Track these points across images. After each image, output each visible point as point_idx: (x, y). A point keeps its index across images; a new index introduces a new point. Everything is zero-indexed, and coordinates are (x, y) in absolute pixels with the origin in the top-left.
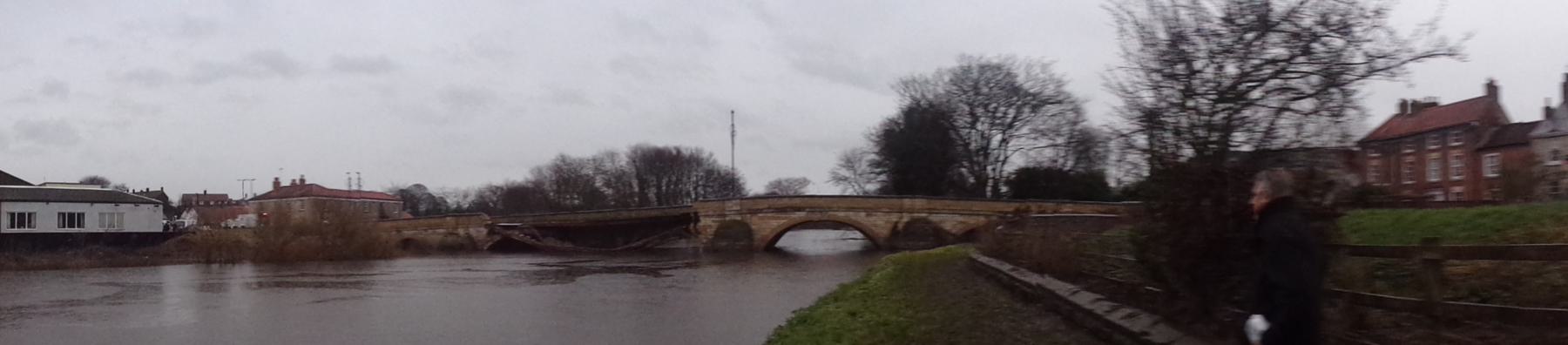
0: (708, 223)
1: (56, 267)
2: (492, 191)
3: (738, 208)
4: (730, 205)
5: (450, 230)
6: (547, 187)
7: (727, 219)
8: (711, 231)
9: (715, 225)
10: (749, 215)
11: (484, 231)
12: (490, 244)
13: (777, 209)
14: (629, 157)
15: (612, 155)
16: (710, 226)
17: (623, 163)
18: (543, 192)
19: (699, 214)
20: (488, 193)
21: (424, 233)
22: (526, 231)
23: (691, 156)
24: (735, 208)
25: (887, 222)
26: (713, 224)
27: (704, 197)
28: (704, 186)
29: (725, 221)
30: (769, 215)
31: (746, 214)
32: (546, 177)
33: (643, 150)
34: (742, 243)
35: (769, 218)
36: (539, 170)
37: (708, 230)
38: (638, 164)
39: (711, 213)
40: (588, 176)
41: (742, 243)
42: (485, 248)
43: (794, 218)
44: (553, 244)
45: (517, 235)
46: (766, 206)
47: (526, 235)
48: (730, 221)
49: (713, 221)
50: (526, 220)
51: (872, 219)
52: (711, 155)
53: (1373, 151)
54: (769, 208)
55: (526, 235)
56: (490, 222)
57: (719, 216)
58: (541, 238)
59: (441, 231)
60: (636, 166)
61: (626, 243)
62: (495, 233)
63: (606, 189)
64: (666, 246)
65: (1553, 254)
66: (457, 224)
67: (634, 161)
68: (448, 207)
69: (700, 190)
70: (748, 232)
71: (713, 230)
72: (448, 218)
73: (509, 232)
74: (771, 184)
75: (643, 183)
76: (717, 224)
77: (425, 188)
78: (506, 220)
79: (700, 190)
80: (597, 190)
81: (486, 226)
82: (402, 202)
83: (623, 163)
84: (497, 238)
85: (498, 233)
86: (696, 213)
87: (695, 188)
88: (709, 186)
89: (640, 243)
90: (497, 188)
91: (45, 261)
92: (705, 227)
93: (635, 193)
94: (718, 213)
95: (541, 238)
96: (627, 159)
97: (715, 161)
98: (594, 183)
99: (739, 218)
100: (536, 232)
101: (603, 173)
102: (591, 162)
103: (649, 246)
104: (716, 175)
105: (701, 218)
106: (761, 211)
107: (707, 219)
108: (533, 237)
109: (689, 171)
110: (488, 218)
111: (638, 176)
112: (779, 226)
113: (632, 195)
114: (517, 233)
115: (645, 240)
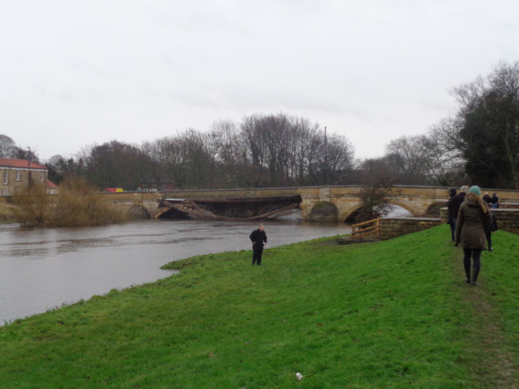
0: (308, 203)
3: (328, 193)
4: (323, 191)
5: (137, 203)
7: (321, 200)
8: (309, 209)
9: (313, 204)
10: (335, 198)
11: (157, 205)
12: (160, 214)
13: (352, 194)
15: (227, 127)
16: (309, 205)
19: (302, 197)
21: (113, 204)
24: (325, 193)
25: (424, 205)
29: (319, 202)
30: (349, 198)
31: (333, 197)
33: (257, 122)
34: (330, 217)
35: (349, 200)
37: (308, 208)
41: (330, 217)
42: (156, 217)
45: (181, 208)
46: (347, 192)
47: (188, 208)
49: (311, 202)
51: (412, 202)
54: (349, 194)
55: (188, 208)
57: (315, 198)
59: (128, 203)
61: (255, 214)
66: (142, 199)
70: (335, 210)
71: (311, 207)
73: (176, 206)
74: (393, 143)
75: (256, 153)
76: (313, 204)
77: (9, 140)
81: (158, 201)
82: (47, 171)
84: (165, 210)
85: (166, 206)
91: (237, 224)
92: (306, 206)
94: (314, 196)
96: (241, 130)
99: (328, 200)
100: (195, 205)
105: (304, 200)
106: (343, 195)
107: (307, 200)
111: (253, 147)
112: (355, 206)
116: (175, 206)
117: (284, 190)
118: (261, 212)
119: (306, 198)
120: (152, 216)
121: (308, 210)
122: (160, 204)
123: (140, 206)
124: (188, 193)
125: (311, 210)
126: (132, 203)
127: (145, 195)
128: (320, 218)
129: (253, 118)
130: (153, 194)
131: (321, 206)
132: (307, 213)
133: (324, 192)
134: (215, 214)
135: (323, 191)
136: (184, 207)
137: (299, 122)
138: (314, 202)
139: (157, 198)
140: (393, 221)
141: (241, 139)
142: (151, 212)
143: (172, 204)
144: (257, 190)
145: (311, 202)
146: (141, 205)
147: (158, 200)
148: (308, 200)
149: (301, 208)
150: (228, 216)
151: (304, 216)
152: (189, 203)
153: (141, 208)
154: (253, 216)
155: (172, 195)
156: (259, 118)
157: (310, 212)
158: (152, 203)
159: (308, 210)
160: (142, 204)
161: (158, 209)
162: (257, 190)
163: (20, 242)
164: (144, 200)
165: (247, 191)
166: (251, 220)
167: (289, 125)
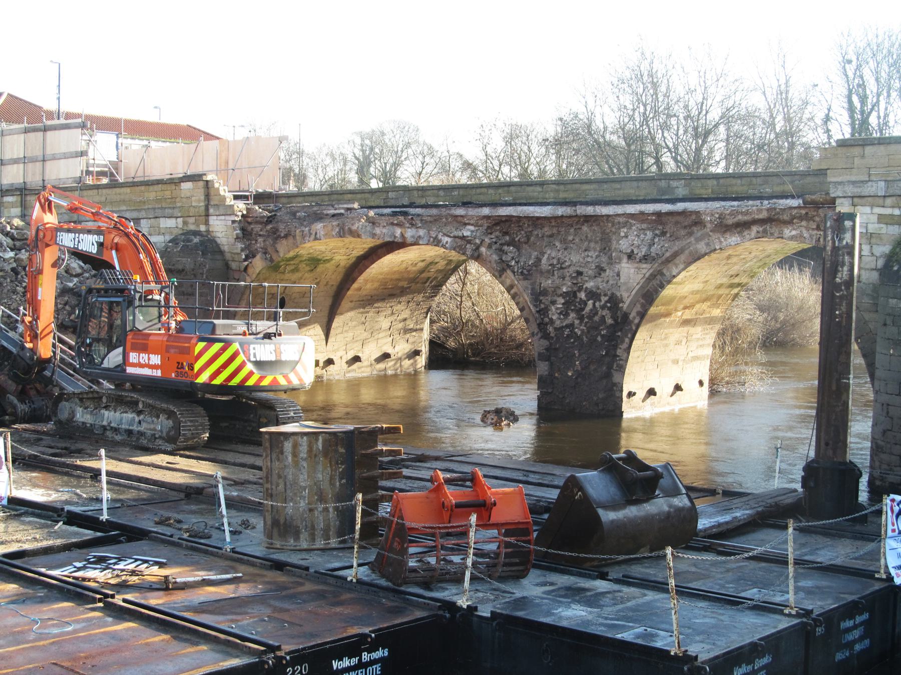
26: (884, 229)
49: (881, 218)
125: (881, 263)
146: (203, 228)
160: (207, 223)
164: (211, 211)
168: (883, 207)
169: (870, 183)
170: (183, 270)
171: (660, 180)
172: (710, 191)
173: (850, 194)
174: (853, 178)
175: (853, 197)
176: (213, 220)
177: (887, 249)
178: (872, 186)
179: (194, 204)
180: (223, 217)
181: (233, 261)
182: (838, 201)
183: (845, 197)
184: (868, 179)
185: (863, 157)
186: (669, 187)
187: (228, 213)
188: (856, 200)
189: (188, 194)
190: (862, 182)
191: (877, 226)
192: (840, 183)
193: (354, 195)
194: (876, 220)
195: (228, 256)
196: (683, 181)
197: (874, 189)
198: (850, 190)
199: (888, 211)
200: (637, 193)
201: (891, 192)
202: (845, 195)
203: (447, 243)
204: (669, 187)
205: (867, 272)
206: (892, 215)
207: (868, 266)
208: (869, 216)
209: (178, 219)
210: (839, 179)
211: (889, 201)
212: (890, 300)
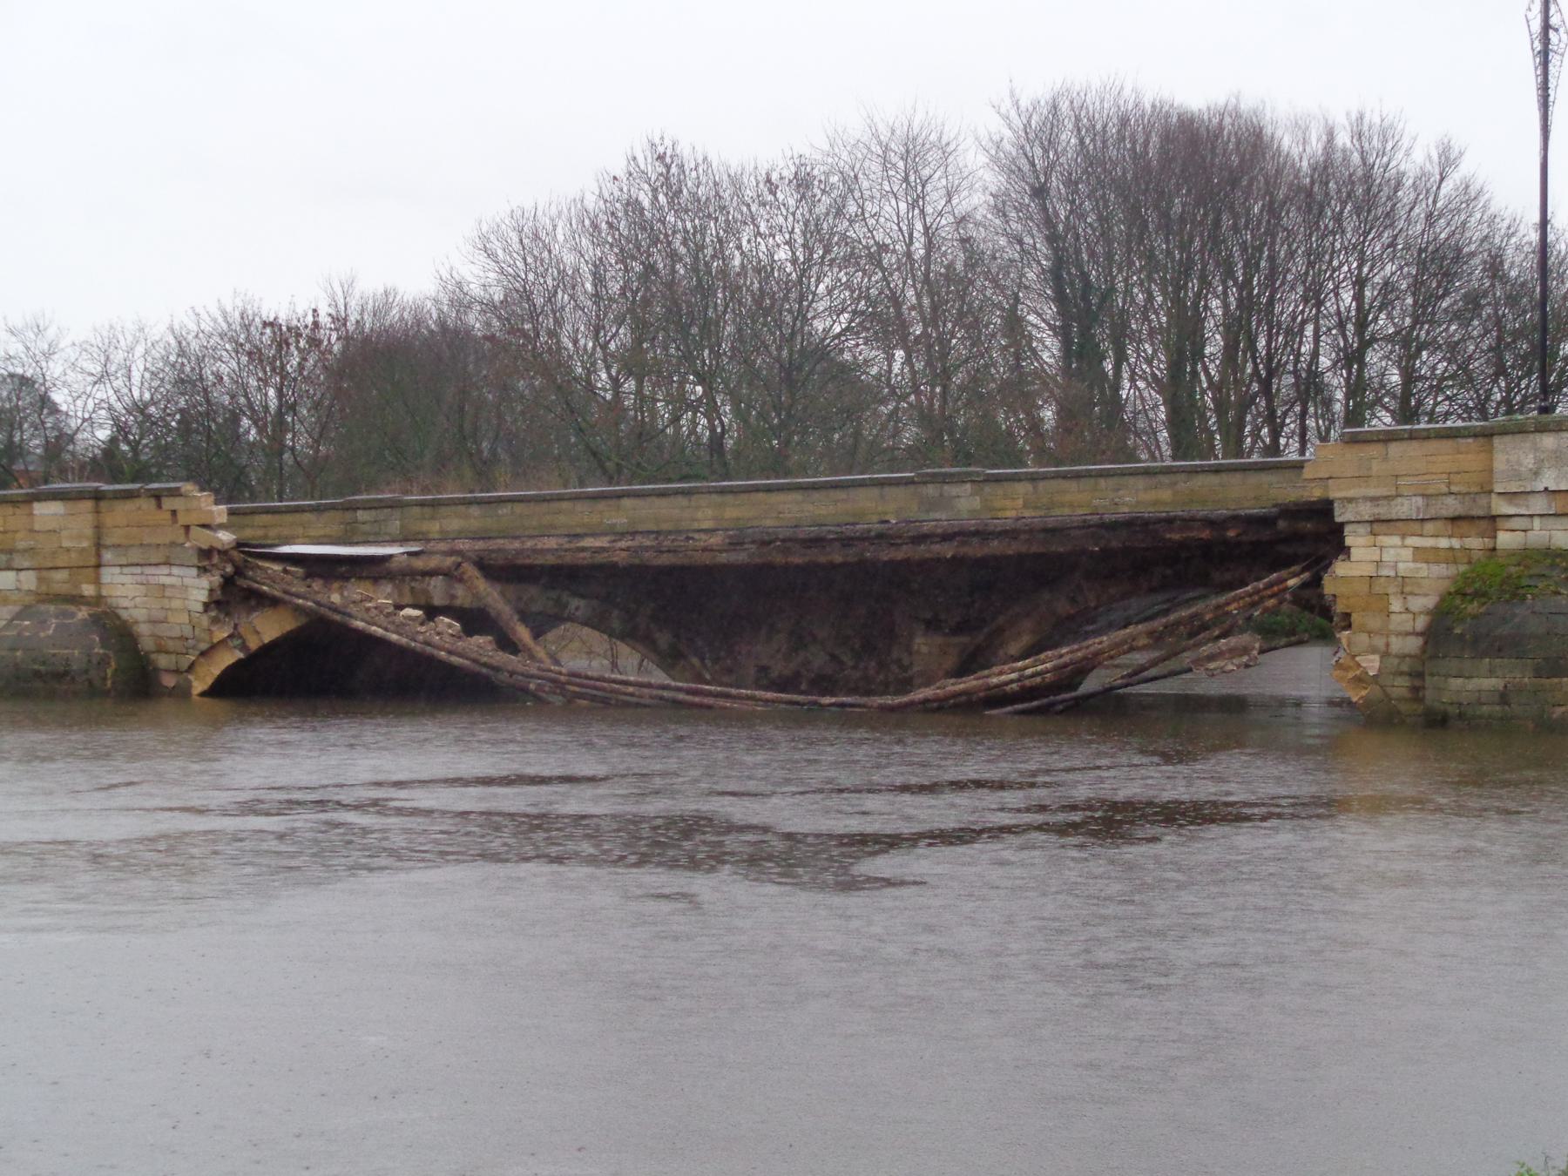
1: (817, 542)
2: (255, 355)
6: (575, 336)
7: (1505, 539)
9: (1433, 580)
11: (198, 589)
12: (227, 659)
14: (1012, 170)
16: (1405, 585)
17: (975, 201)
18: (551, 365)
20: (227, 367)
22: (437, 590)
23: (1325, 168)
26: (1423, 570)
27: (1407, 412)
28: (1408, 347)
32: (568, 281)
36: (534, 240)
37: (1396, 605)
38: (406, 315)
39: (1406, 507)
40: (764, 271)
42: (199, 686)
43: (515, 632)
44: (596, 666)
47: (431, 612)
48: (1526, 556)
49: (1420, 554)
50: (434, 527)
52: (1447, 161)
53: (393, 565)
55: (431, 612)
56: (225, 537)
58: (523, 633)
60: (1049, 222)
62: (259, 600)
63: (866, 352)
64: (1204, 684)
65: (4, 879)
67: (1040, 192)
68: (58, 444)
69: (1382, 366)
71: (1424, 602)
72: (45, 510)
78: (320, 524)
79: (1382, 366)
80: (821, 353)
83: (975, 201)
84: (268, 628)
85: (274, 602)
86: (1323, 510)
87: (1352, 358)
88: (1299, 348)
89: (1043, 666)
90: (283, 336)
93: (1039, 374)
94: (1452, 506)
95: (523, 633)
96: (993, 180)
97: (1469, 196)
98: (802, 316)
100: (492, 596)
101: (850, 260)
102: (787, 196)
103: (1090, 685)
104: (1475, 274)
105: (1355, 539)
108: (474, 620)
109: (1314, 256)
110: (220, 512)
113: (1020, 391)
114: (383, 596)
115: (1067, 653)
116: (336, 598)
117: (1200, 481)
118: (1014, 648)
119: (1378, 524)
120: (169, 681)
121: (1400, 621)
122: (228, 582)
123: (77, 599)
124: (504, 510)
125: (1421, 623)
126: (29, 580)
127: (119, 515)
128: (1504, 697)
129: (1064, 106)
130: (168, 503)
131: (1514, 591)
132: (1385, 655)
133: (1536, 473)
134: (671, 659)
135: (1529, 461)
136: (400, 607)
137: (1343, 139)
138: (1451, 556)
139: (203, 538)
140: (935, 705)
141: (993, 239)
142: (161, 650)
143: (317, 585)
144: (998, 479)
145: (1420, 554)
146: (88, 590)
147: (206, 553)
148: (1396, 540)
149: (1339, 608)
150: (765, 679)
151: (1360, 680)
152: (450, 575)
153: (83, 613)
154: (961, 671)
155: (395, 526)
156: (1103, 108)
157: (1413, 644)
158: (163, 576)
159: (1400, 621)
160: (97, 581)
161: (205, 621)
162: (998, 479)
163: (492, 772)
164: (108, 556)
165: (931, 490)
166: (926, 707)
167: (1283, 165)
168: (1421, 535)
169: (1399, 500)
170: (66, 673)
171: (925, 483)
172: (1020, 502)
173: (1367, 518)
174: (1372, 492)
175: (1371, 522)
176: (109, 575)
177: (1430, 602)
178: (1402, 505)
179: (66, 544)
180: (138, 570)
181: (159, 651)
182: (1347, 529)
183: (1359, 522)
184: (1394, 493)
185: (1385, 459)
186: (941, 495)
187: (153, 561)
188: (1375, 526)
189: (52, 525)
190: (1386, 497)
191: (1411, 565)
192: (1350, 500)
193: (277, 517)
194: (1411, 558)
195: (147, 644)
196: (968, 486)
197: (1405, 508)
198: (1366, 511)
199: (1428, 542)
200: (880, 508)
201: (1432, 513)
202: (1359, 518)
203: (577, 609)
204: (941, 495)
205: (1400, 638)
206: (1437, 549)
207: (1401, 629)
208: (1399, 550)
209: (23, 574)
210: (1351, 493)
211: (1429, 527)
212: (1452, 680)
